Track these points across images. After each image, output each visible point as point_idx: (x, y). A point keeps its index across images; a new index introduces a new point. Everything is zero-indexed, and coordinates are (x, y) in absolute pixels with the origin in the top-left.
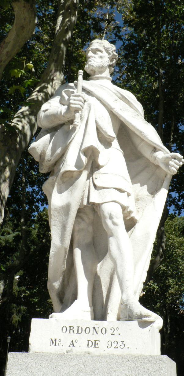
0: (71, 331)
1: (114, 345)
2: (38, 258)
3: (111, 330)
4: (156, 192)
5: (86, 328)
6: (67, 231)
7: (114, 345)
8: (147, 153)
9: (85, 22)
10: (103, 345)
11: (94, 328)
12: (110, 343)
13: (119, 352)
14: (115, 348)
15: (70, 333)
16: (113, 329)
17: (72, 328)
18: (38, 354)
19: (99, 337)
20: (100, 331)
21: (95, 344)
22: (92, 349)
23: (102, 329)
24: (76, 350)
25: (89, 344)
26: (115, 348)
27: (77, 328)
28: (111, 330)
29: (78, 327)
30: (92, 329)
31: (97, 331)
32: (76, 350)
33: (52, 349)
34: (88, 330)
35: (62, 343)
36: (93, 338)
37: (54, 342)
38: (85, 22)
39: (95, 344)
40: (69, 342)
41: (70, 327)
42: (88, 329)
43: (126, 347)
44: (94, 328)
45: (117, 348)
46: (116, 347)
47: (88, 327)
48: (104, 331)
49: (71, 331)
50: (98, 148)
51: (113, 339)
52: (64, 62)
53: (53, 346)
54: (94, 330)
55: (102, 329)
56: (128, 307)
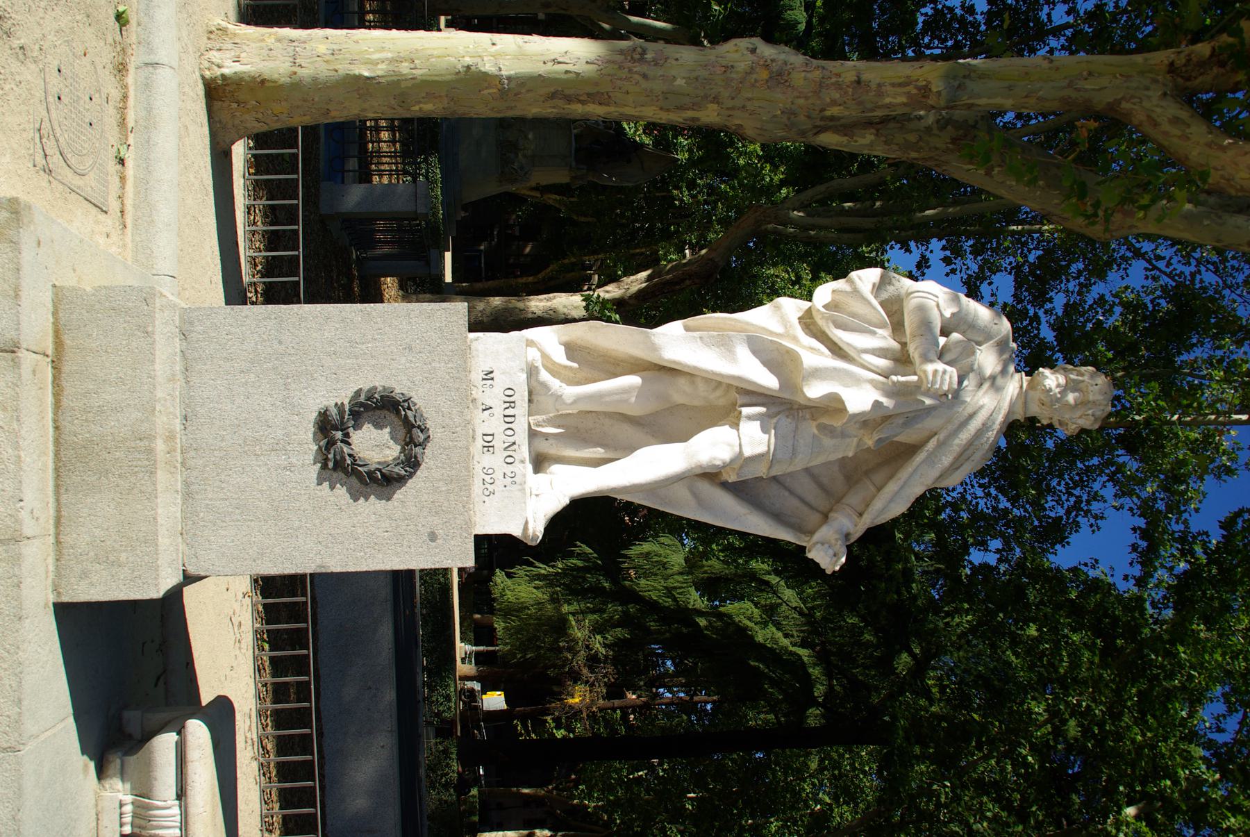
1: (488, 478)
4: (267, 84)
7: (488, 478)
8: (854, 499)
10: (487, 460)
12: (490, 471)
13: (477, 487)
18: (465, 353)
19: (500, 455)
21: (489, 447)
22: (480, 442)
24: (479, 416)
30: (511, 439)
32: (479, 416)
33: (476, 376)
35: (487, 390)
36: (498, 443)
37: (488, 376)
39: (489, 447)
40: (489, 403)
43: (486, 499)
48: (510, 392)
50: (691, 321)
51: (498, 475)
52: (928, 212)
53: (482, 375)
56: (518, 420)
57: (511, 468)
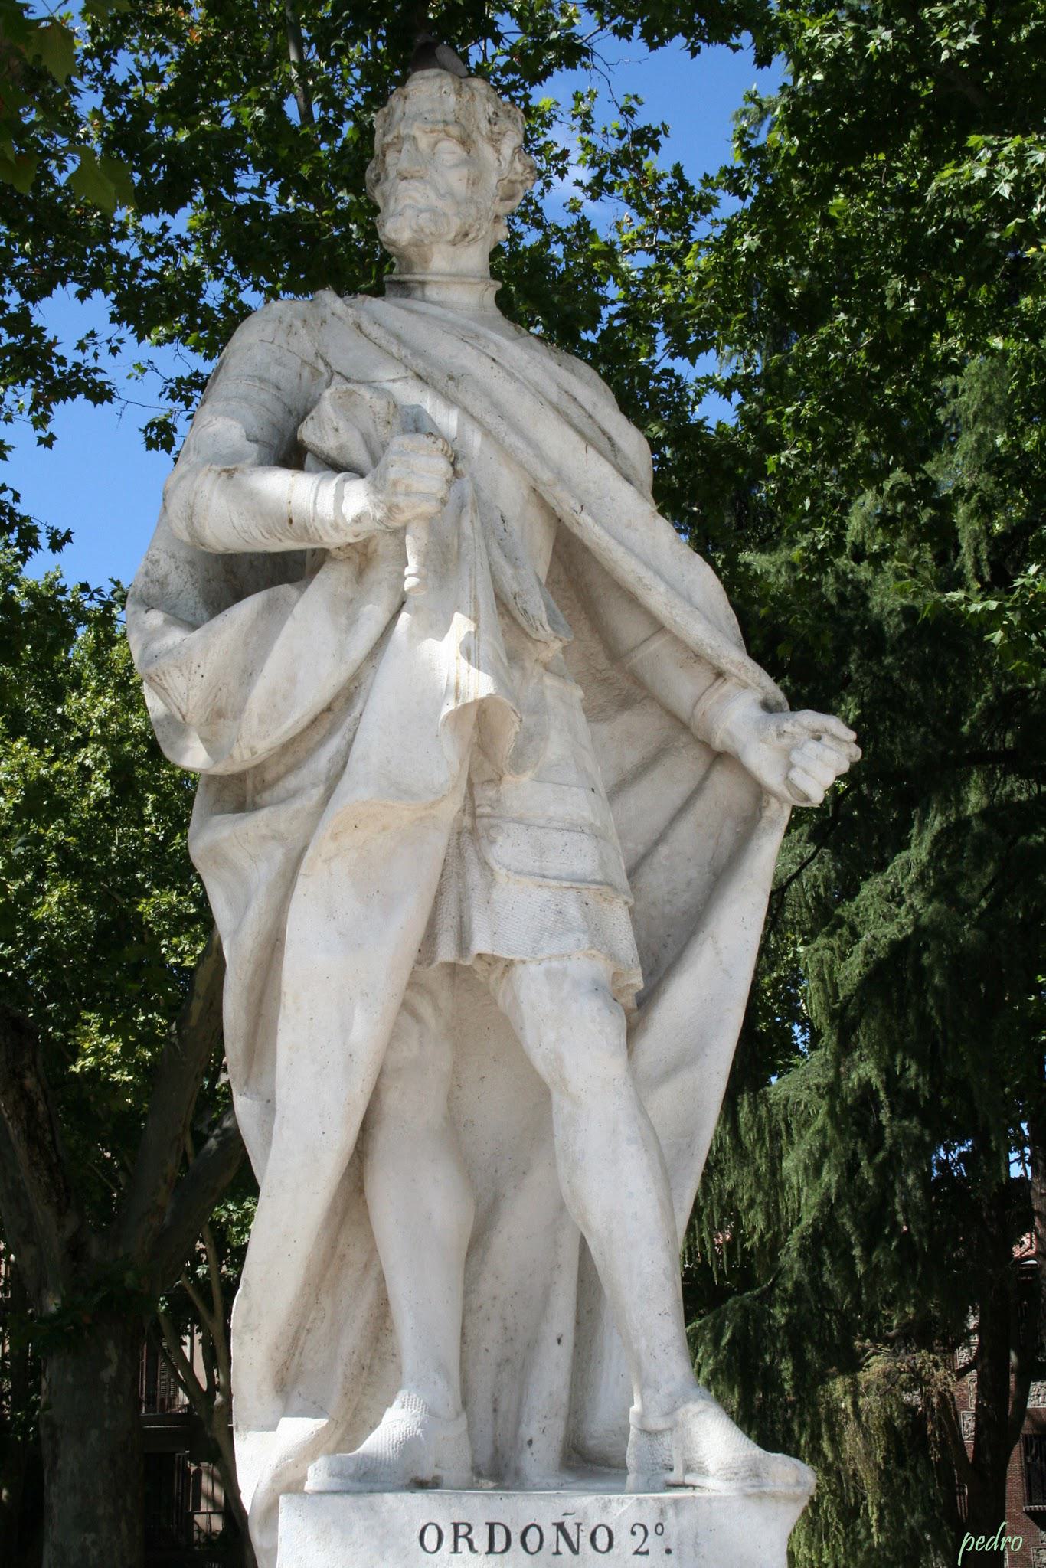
0: (463, 1543)
2: (200, 1245)
3: (633, 1533)
5: (527, 1529)
6: (341, 448)
9: (927, 1139)
11: (560, 1527)
14: (637, 1552)
15: (456, 1550)
16: (639, 1530)
17: (463, 1530)
20: (588, 1543)
23: (593, 1534)
25: (580, 425)
26: (637, 1552)
27: (487, 1529)
28: (633, 1533)
29: (491, 1526)
30: (550, 1533)
31: (574, 1540)
34: (533, 1538)
38: (927, 1139)
41: (456, 1526)
42: (533, 1531)
44: (560, 1527)
45: (647, 1553)
46: (643, 1549)
47: (533, 1525)
48: (602, 1540)
49: (463, 1543)
54: (562, 1539)
55: (593, 1534)
57: (622, 1537)
